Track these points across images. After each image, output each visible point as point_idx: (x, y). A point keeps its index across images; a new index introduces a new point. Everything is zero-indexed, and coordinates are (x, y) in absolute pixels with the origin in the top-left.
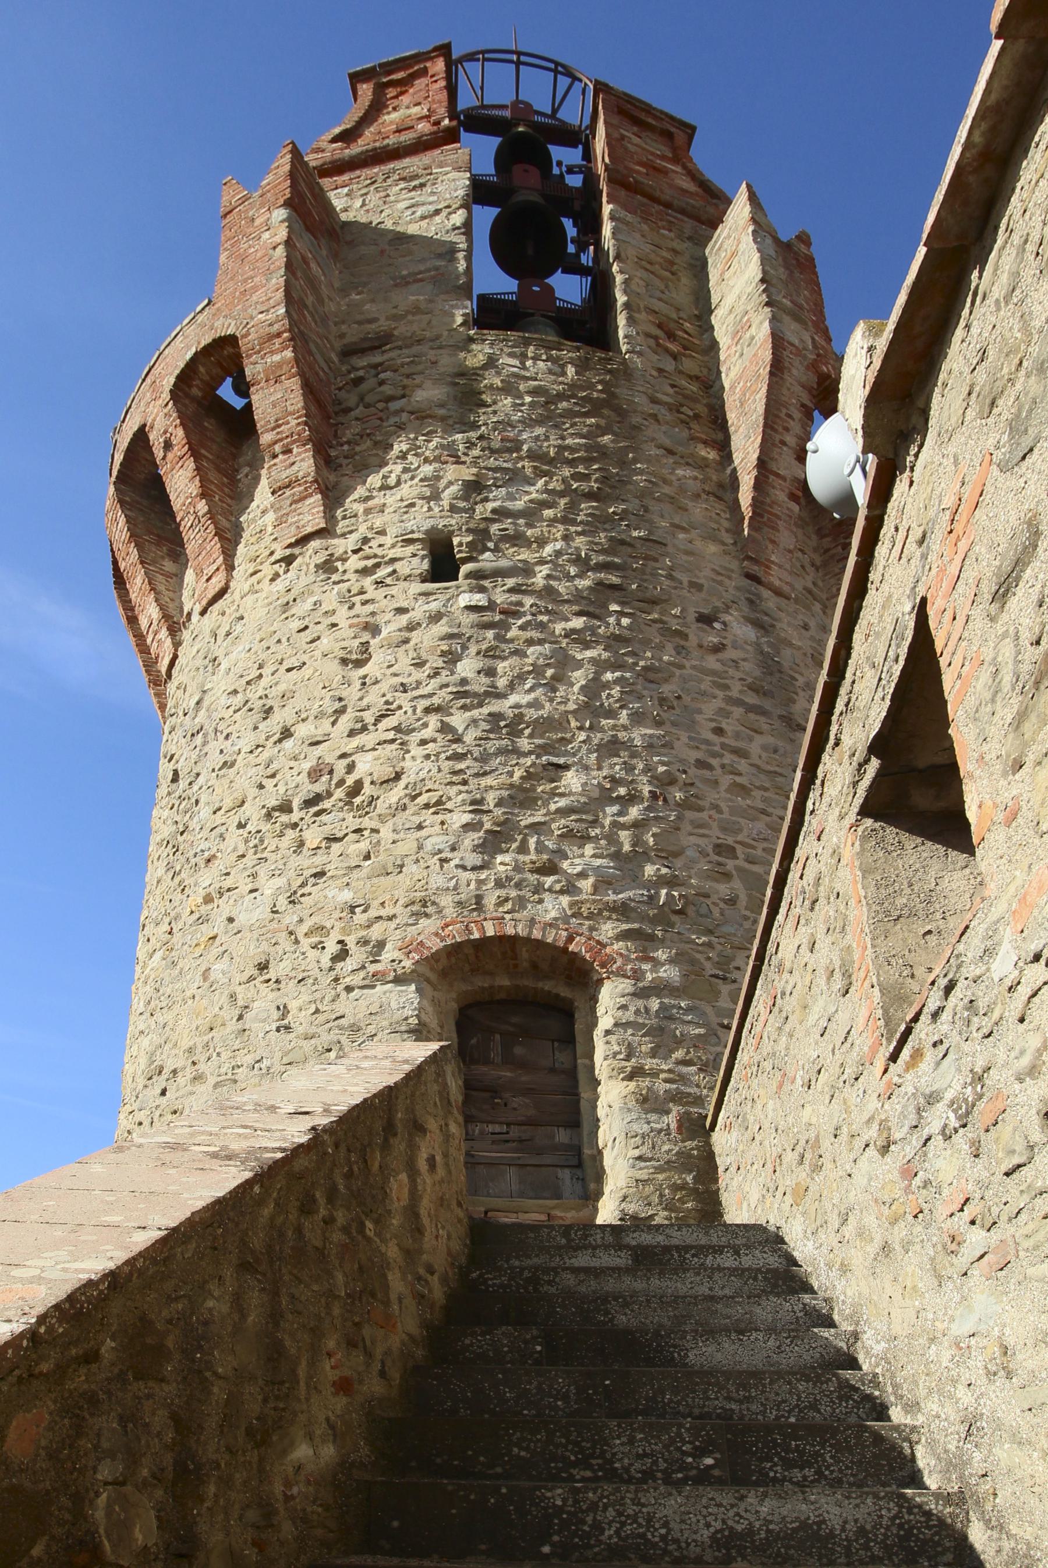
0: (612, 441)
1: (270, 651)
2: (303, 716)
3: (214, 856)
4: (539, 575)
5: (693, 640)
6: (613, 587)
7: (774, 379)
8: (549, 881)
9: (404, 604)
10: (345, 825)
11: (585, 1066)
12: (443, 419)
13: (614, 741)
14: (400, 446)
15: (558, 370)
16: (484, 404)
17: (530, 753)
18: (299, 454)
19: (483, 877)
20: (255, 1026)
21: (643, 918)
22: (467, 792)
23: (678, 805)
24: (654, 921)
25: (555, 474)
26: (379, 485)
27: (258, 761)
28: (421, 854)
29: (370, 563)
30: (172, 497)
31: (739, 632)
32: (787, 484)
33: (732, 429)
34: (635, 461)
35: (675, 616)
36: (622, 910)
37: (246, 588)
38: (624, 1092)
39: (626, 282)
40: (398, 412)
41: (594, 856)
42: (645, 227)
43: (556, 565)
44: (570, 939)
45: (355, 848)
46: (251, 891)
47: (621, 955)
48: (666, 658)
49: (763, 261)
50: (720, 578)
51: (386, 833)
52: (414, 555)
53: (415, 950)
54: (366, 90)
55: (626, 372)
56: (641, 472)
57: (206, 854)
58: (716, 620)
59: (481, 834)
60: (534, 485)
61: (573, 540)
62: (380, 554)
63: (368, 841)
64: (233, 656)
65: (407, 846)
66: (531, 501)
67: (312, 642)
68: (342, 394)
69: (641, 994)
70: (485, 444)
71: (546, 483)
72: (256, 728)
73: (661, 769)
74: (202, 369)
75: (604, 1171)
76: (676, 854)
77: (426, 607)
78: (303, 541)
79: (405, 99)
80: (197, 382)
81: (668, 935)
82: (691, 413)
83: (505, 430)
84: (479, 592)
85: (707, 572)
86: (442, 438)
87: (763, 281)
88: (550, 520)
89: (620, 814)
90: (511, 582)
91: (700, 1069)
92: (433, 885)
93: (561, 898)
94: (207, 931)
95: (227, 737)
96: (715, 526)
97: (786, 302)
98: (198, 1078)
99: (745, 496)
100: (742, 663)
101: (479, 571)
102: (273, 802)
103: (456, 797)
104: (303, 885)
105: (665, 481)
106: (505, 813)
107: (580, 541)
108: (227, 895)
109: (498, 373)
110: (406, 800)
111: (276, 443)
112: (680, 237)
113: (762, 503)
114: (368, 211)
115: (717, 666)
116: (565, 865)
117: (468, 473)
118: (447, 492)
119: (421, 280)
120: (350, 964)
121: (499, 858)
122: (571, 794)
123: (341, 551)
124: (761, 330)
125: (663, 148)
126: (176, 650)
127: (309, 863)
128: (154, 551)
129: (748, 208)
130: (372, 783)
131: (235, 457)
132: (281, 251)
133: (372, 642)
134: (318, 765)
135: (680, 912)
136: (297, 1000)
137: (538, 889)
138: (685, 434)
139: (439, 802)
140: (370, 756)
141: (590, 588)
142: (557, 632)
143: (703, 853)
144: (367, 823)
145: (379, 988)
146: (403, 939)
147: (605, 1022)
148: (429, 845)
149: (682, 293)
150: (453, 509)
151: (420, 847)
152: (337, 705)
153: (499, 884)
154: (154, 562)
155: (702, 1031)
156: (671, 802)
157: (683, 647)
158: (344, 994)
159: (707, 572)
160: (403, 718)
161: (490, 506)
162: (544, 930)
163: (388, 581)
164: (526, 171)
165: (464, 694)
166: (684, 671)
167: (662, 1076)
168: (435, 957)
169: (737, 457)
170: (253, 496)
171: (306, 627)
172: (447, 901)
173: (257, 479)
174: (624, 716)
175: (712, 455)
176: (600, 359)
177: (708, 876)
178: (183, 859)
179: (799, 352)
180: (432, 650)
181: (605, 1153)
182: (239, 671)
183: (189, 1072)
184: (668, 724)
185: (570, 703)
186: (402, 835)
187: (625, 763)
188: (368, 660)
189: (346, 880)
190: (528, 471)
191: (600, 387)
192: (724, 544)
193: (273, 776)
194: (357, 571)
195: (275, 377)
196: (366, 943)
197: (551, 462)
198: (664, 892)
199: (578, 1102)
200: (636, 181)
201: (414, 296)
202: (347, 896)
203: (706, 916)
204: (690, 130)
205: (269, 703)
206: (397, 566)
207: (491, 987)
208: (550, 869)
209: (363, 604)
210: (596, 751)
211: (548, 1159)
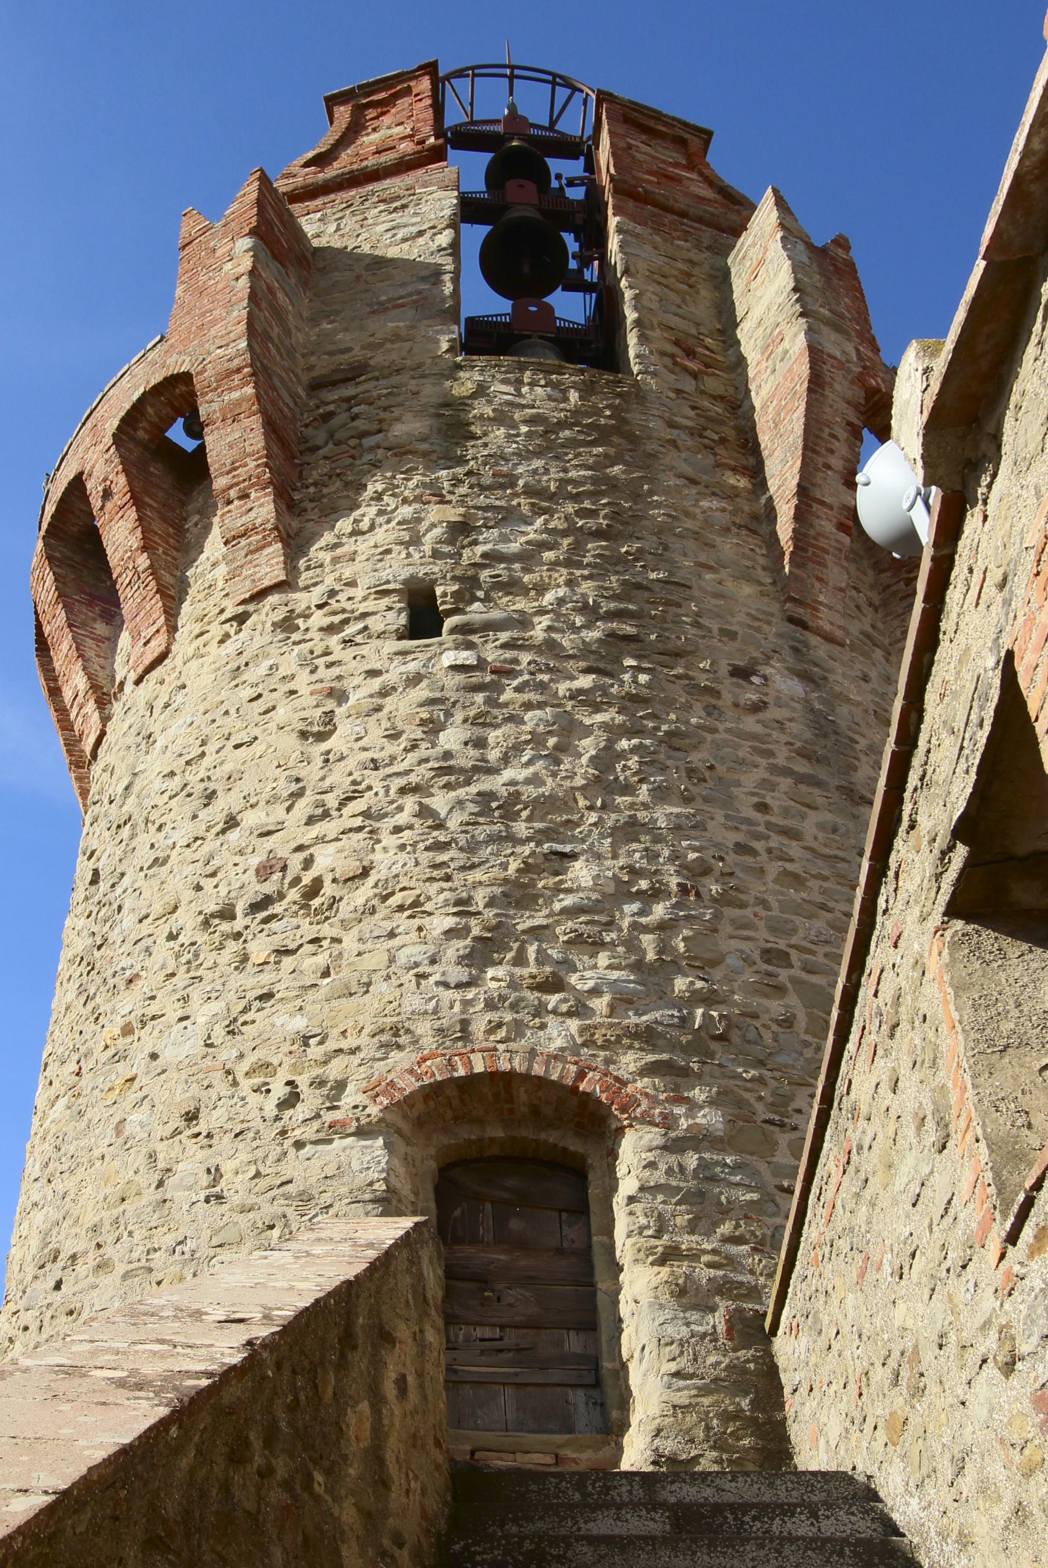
0: (623, 472)
2: (253, 801)
3: (137, 976)
5: (727, 698)
6: (627, 638)
7: (814, 396)
8: (553, 1000)
9: (377, 666)
10: (299, 933)
11: (603, 1245)
12: (425, 454)
14: (374, 486)
15: (556, 394)
16: (474, 437)
17: (529, 839)
18: (258, 498)
19: (470, 996)
21: (673, 1046)
22: (451, 889)
23: (715, 900)
24: (687, 1050)
25: (556, 511)
26: (349, 530)
27: (196, 856)
28: (391, 970)
29: (337, 619)
30: (109, 552)
32: (835, 513)
33: (765, 454)
34: (651, 493)
35: (704, 670)
36: (647, 1037)
37: (190, 651)
39: (636, 297)
40: (372, 449)
41: (610, 967)
42: (658, 239)
43: (558, 615)
44: (581, 1075)
45: (311, 962)
46: (181, 1019)
47: (647, 1095)
48: (694, 721)
49: (795, 269)
50: (756, 624)
51: (350, 943)
53: (384, 1093)
54: (343, 113)
55: (638, 394)
57: (128, 973)
58: (754, 673)
59: (468, 941)
61: (579, 585)
63: (327, 953)
64: (171, 732)
65: (376, 959)
66: (528, 543)
67: (266, 712)
68: (309, 431)
70: (474, 480)
71: (546, 522)
72: (195, 817)
73: (692, 856)
74: (150, 410)
76: (714, 963)
77: (403, 668)
78: (260, 595)
79: (386, 120)
80: (145, 424)
81: (707, 1068)
82: (716, 437)
83: (497, 464)
85: (741, 617)
87: (795, 290)
89: (642, 913)
90: (504, 636)
92: (407, 1009)
93: (569, 1021)
94: (124, 1070)
95: (160, 828)
96: (749, 564)
98: (102, 1266)
99: (785, 529)
100: (788, 724)
101: (467, 624)
102: (212, 907)
103: (438, 895)
104: (246, 1010)
105: (687, 514)
106: (497, 915)
107: (587, 588)
109: (490, 402)
110: (375, 902)
111: (231, 487)
112: (698, 247)
113: (806, 535)
114: (343, 236)
115: (759, 729)
116: (573, 979)
117: (453, 514)
119: (402, 306)
120: (301, 1111)
121: (491, 972)
122: (579, 889)
123: (303, 606)
124: (796, 342)
125: (675, 155)
126: (104, 726)
127: (253, 982)
128: (85, 612)
129: (775, 214)
130: (334, 881)
131: (183, 504)
132: (244, 282)
133: (338, 711)
134: (268, 861)
135: (722, 1038)
137: (540, 1010)
139: (416, 904)
140: (332, 847)
142: (561, 693)
143: (749, 961)
144: (327, 930)
145: (338, 1143)
146: (369, 1078)
147: (627, 1186)
148: (402, 957)
149: (702, 307)
150: (436, 554)
151: (392, 960)
152: (294, 787)
153: (490, 1005)
154: (84, 625)
155: (755, 1196)
156: (706, 897)
157: (715, 707)
158: (292, 1151)
159: (741, 617)
161: (480, 549)
162: (547, 1063)
163: (359, 639)
165: (448, 770)
166: (717, 736)
167: (705, 1258)
168: (409, 1101)
169: (773, 485)
171: (260, 696)
172: (424, 1028)
176: (608, 382)
177: (755, 990)
178: (99, 980)
179: (841, 365)
180: (408, 719)
181: (632, 1366)
183: (92, 1259)
184: (699, 800)
186: (369, 945)
187: (646, 849)
188: (331, 733)
189: (298, 1003)
190: (525, 509)
191: (608, 413)
192: (760, 584)
193: (213, 875)
194: (321, 629)
196: (322, 1083)
197: (552, 497)
198: (699, 1012)
199: (594, 1294)
200: (646, 191)
201: (392, 323)
202: (300, 1023)
203: (756, 1043)
204: (706, 136)
205: (212, 786)
206: (370, 621)
207: (481, 1140)
208: (554, 984)
210: (611, 835)
211: (556, 1376)
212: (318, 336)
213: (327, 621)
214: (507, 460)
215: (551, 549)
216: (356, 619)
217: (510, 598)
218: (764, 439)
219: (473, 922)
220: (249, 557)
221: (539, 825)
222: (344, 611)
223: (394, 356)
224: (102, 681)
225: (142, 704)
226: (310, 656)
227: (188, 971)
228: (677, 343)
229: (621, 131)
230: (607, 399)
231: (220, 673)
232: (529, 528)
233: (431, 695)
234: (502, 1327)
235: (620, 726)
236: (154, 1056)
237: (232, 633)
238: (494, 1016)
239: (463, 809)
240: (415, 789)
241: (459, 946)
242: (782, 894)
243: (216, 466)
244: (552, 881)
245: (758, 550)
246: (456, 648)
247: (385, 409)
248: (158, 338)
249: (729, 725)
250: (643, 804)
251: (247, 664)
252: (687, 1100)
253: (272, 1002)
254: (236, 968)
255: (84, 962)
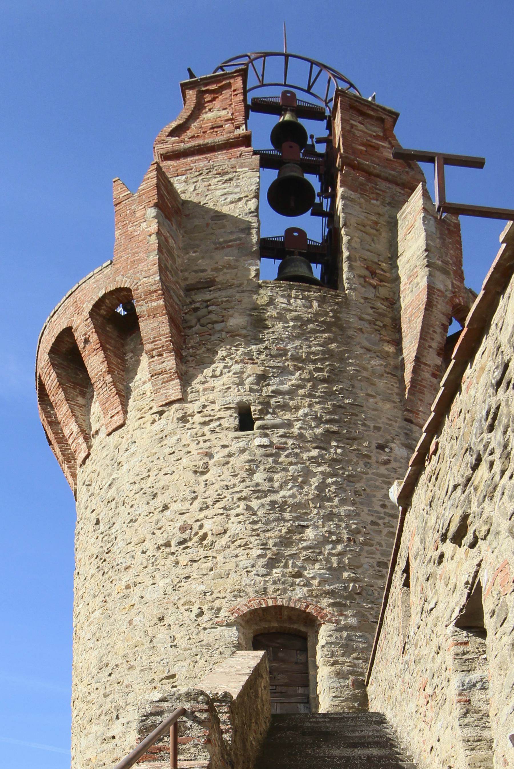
0: (337, 347)
1: (154, 463)
2: (175, 499)
3: (130, 567)
4: (296, 427)
5: (374, 459)
6: (334, 432)
7: (427, 312)
8: (298, 581)
9: (226, 443)
10: (199, 554)
11: (312, 661)
12: (245, 337)
13: (331, 513)
14: (222, 353)
15: (308, 304)
16: (267, 327)
17: (290, 520)
18: (167, 357)
19: (267, 579)
20: (159, 645)
21: (341, 596)
22: (259, 539)
23: (361, 544)
24: (346, 598)
25: (305, 369)
26: (210, 375)
27: (151, 520)
28: (237, 569)
29: (207, 419)
31: (398, 453)
32: (431, 369)
33: (404, 334)
34: (349, 358)
35: (365, 447)
36: (332, 594)
37: (137, 426)
38: (329, 671)
39: (349, 242)
41: (320, 569)
42: (362, 200)
43: (304, 421)
44: (307, 607)
45: (206, 565)
46: (152, 584)
47: (330, 613)
48: (359, 470)
50: (391, 422)
51: (220, 558)
52: (231, 416)
53: (236, 612)
54: (191, 94)
55: (346, 302)
56: (352, 365)
57: (124, 565)
58: (387, 447)
59: (266, 559)
60: (294, 375)
61: (314, 407)
62: (212, 414)
63: (211, 562)
64: (132, 463)
65: (231, 565)
66: (292, 385)
67: (177, 460)
68: (188, 317)
69: (339, 630)
70: (268, 352)
71: (300, 375)
72: (148, 503)
73: (354, 526)
74: (107, 301)
75: (319, 703)
76: (358, 567)
77: (237, 445)
79: (217, 104)
80: (104, 307)
81: (353, 604)
82: (381, 325)
83: (278, 343)
84: (265, 437)
85: (384, 420)
86: (245, 348)
87: (426, 250)
88: (302, 396)
89: (333, 549)
90: (281, 431)
91: (364, 662)
92: (243, 583)
93: (303, 588)
94: (128, 602)
95: (132, 507)
96: (390, 392)
97: (439, 263)
98: (131, 668)
99: (408, 376)
101: (265, 425)
102: (161, 542)
103: (254, 542)
104: (179, 582)
105: (365, 369)
106: (277, 550)
107: (317, 408)
108: (138, 586)
109: (275, 308)
110: (230, 543)
111: (154, 350)
112: (383, 204)
113: (417, 380)
115: (385, 472)
116: (305, 573)
117: (259, 370)
118: (248, 380)
120: (205, 618)
121: (275, 571)
122: (309, 540)
123: (191, 411)
125: (376, 129)
126: (89, 450)
127: (182, 572)
128: (74, 393)
129: (421, 201)
130: (212, 534)
131: (123, 345)
132: (154, 238)
133: (210, 462)
134: (184, 525)
135: (359, 594)
136: (180, 634)
138: (378, 338)
139: (246, 544)
140: (211, 521)
141: (322, 434)
142: (304, 458)
143: (372, 567)
144: (210, 553)
145: (219, 628)
146: (230, 607)
148: (241, 565)
149: (381, 246)
150: (251, 390)
151: (237, 566)
152: (193, 495)
153: (275, 582)
154: (73, 399)
155: (366, 645)
156: (357, 542)
157: (368, 463)
158: (202, 631)
159: (384, 420)
160: (227, 503)
161: (271, 388)
162: (295, 603)
163: (217, 429)
164: (291, 147)
165: (258, 491)
166: (368, 476)
167: (346, 664)
168: (245, 615)
169: (405, 352)
170: (136, 371)
171: (174, 452)
172: (250, 590)
173: (138, 362)
174: (336, 500)
175: (391, 349)
176: (332, 295)
177: (374, 577)
179: (442, 294)
180: (241, 468)
181: (320, 696)
182: (137, 472)
184: (358, 503)
185: (310, 495)
186: (228, 560)
187: (336, 524)
188: (207, 472)
189: (201, 580)
190: (291, 368)
191: (331, 314)
192: (394, 402)
193: (160, 529)
194: (200, 423)
195: (153, 314)
196: (212, 609)
197: (303, 361)
198: (351, 585)
199: (308, 676)
200: (359, 163)
202: (202, 588)
203: (371, 595)
204: (395, 116)
206: (222, 421)
207: (269, 627)
209: (204, 442)
210: (322, 518)
212: (189, 260)
213: (203, 420)
214: (283, 341)
215: (302, 388)
216: (216, 420)
217: (283, 412)
218: (404, 326)
219: (268, 552)
220: (164, 384)
221: (294, 514)
222: (210, 415)
223: (228, 277)
224: (85, 428)
225: (112, 446)
226: (195, 436)
227: (153, 566)
228: (367, 268)
229: (347, 118)
230: (331, 306)
231: (153, 439)
232: (293, 377)
233: (250, 458)
234: (276, 686)
235: (329, 473)
236: (142, 597)
237: (157, 419)
238: (276, 586)
239: (264, 508)
240: (244, 499)
241: (264, 561)
242: (387, 540)
243: (146, 338)
244: (299, 536)
245: (395, 385)
246: (261, 437)
247: (225, 309)
248: (109, 262)
249: (374, 471)
250: (336, 506)
251: (166, 436)
252: (345, 615)
253: (190, 579)
254: (174, 566)
255: (99, 558)
